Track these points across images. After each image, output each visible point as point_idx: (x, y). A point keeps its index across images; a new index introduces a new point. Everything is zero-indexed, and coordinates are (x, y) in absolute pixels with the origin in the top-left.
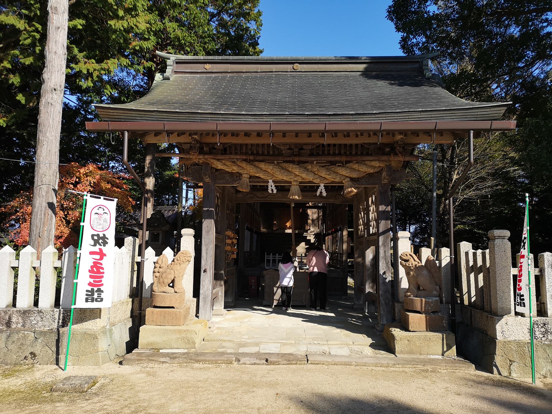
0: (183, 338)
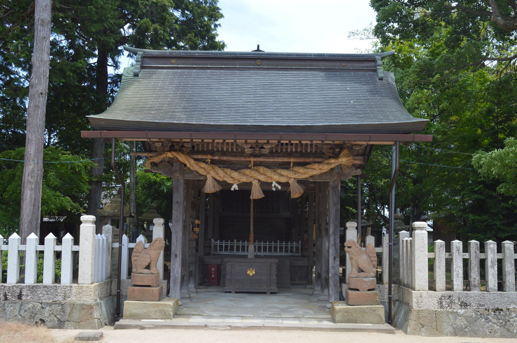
0: (161, 311)
